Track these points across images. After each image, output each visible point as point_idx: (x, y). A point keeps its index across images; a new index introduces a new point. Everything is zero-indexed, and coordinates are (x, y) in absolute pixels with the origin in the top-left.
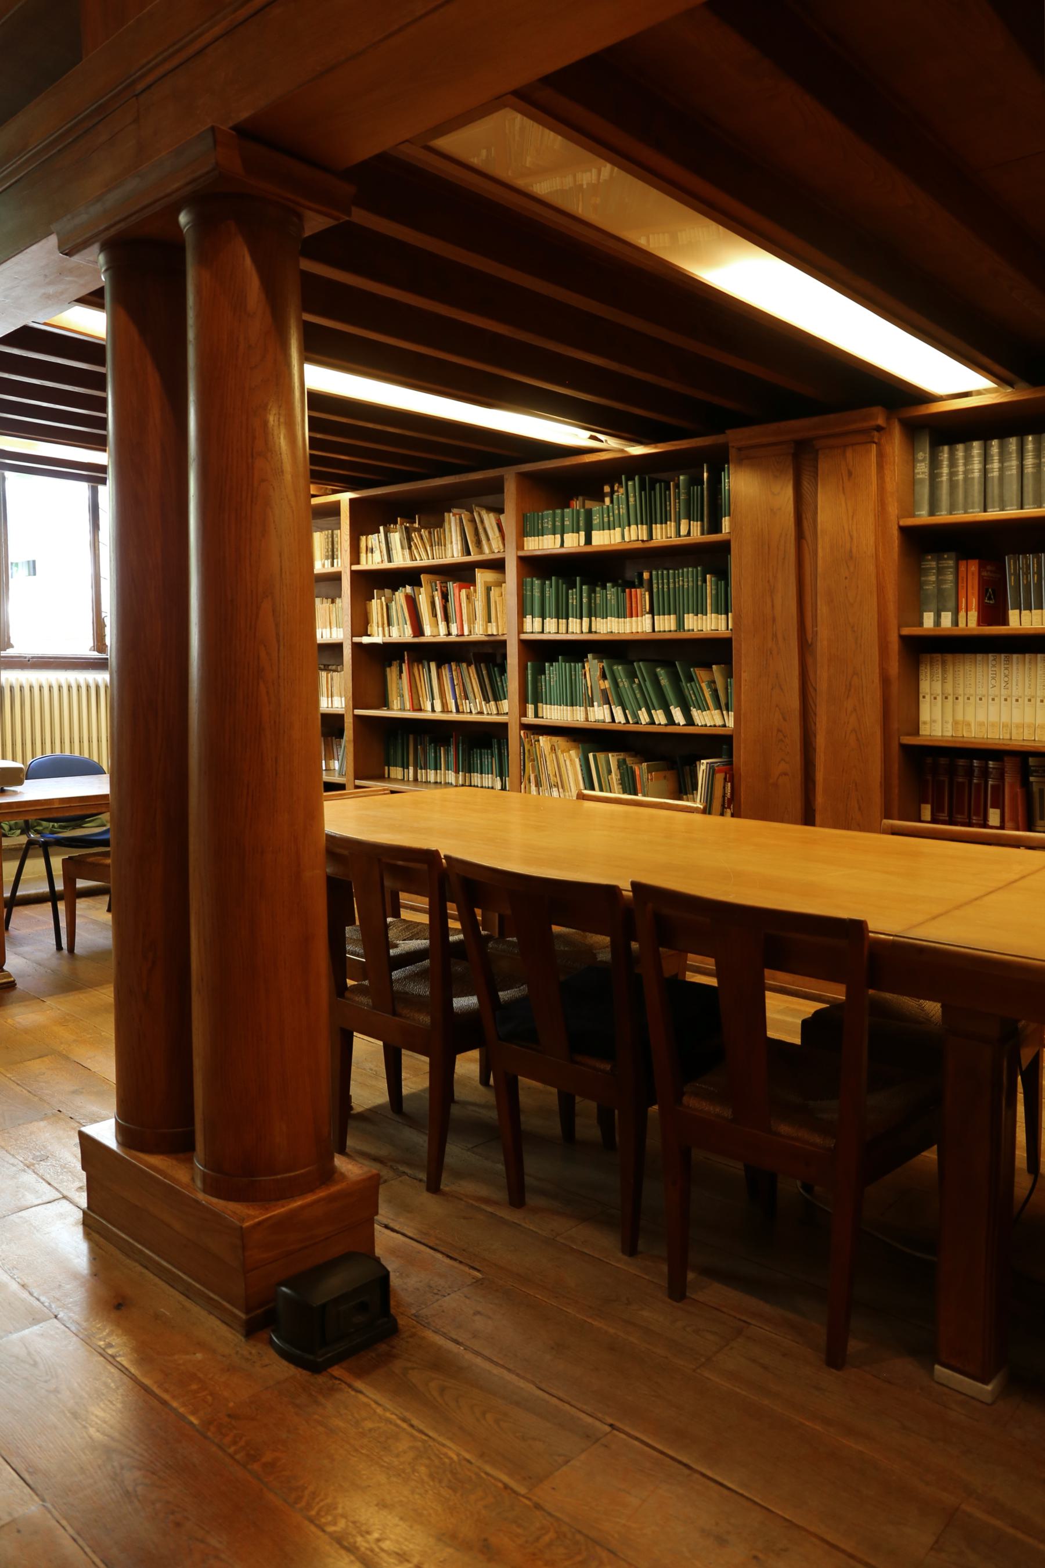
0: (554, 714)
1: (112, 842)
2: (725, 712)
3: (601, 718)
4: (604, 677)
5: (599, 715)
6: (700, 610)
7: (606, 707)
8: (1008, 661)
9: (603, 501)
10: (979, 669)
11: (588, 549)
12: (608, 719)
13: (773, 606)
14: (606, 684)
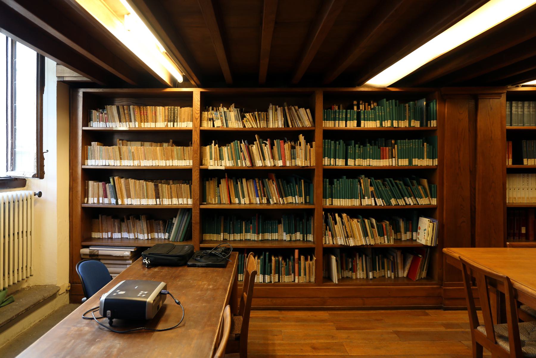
3: (370, 203)
4: (371, 185)
5: (368, 202)
6: (421, 157)
7: (373, 199)
8: (528, 176)
9: (353, 109)
10: (526, 179)
11: (358, 128)
12: (374, 204)
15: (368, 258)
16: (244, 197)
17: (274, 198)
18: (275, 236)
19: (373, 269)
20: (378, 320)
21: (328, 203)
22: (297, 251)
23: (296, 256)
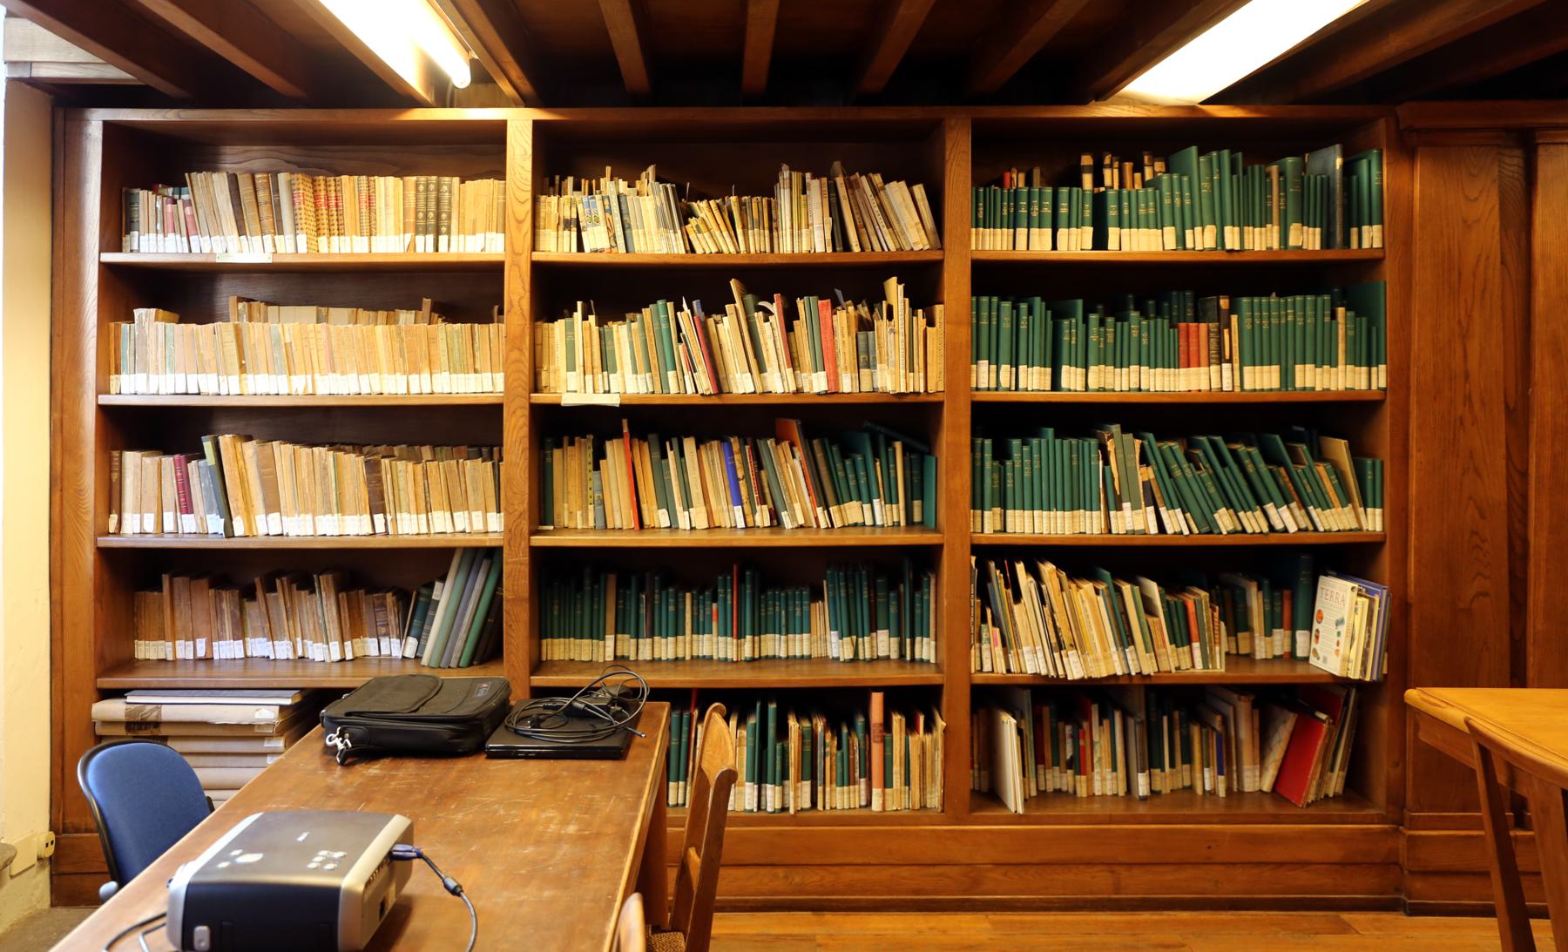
0: (1028, 524)
1: (1551, 912)
2: (1361, 510)
3: (1139, 526)
4: (1144, 460)
5: (1133, 521)
6: (1326, 358)
9: (1079, 184)
11: (1099, 255)
12: (1153, 529)
13: (1465, 356)
14: (1146, 474)
15: (1131, 722)
16: (688, 505)
17: (797, 506)
18: (800, 645)
22: (877, 699)
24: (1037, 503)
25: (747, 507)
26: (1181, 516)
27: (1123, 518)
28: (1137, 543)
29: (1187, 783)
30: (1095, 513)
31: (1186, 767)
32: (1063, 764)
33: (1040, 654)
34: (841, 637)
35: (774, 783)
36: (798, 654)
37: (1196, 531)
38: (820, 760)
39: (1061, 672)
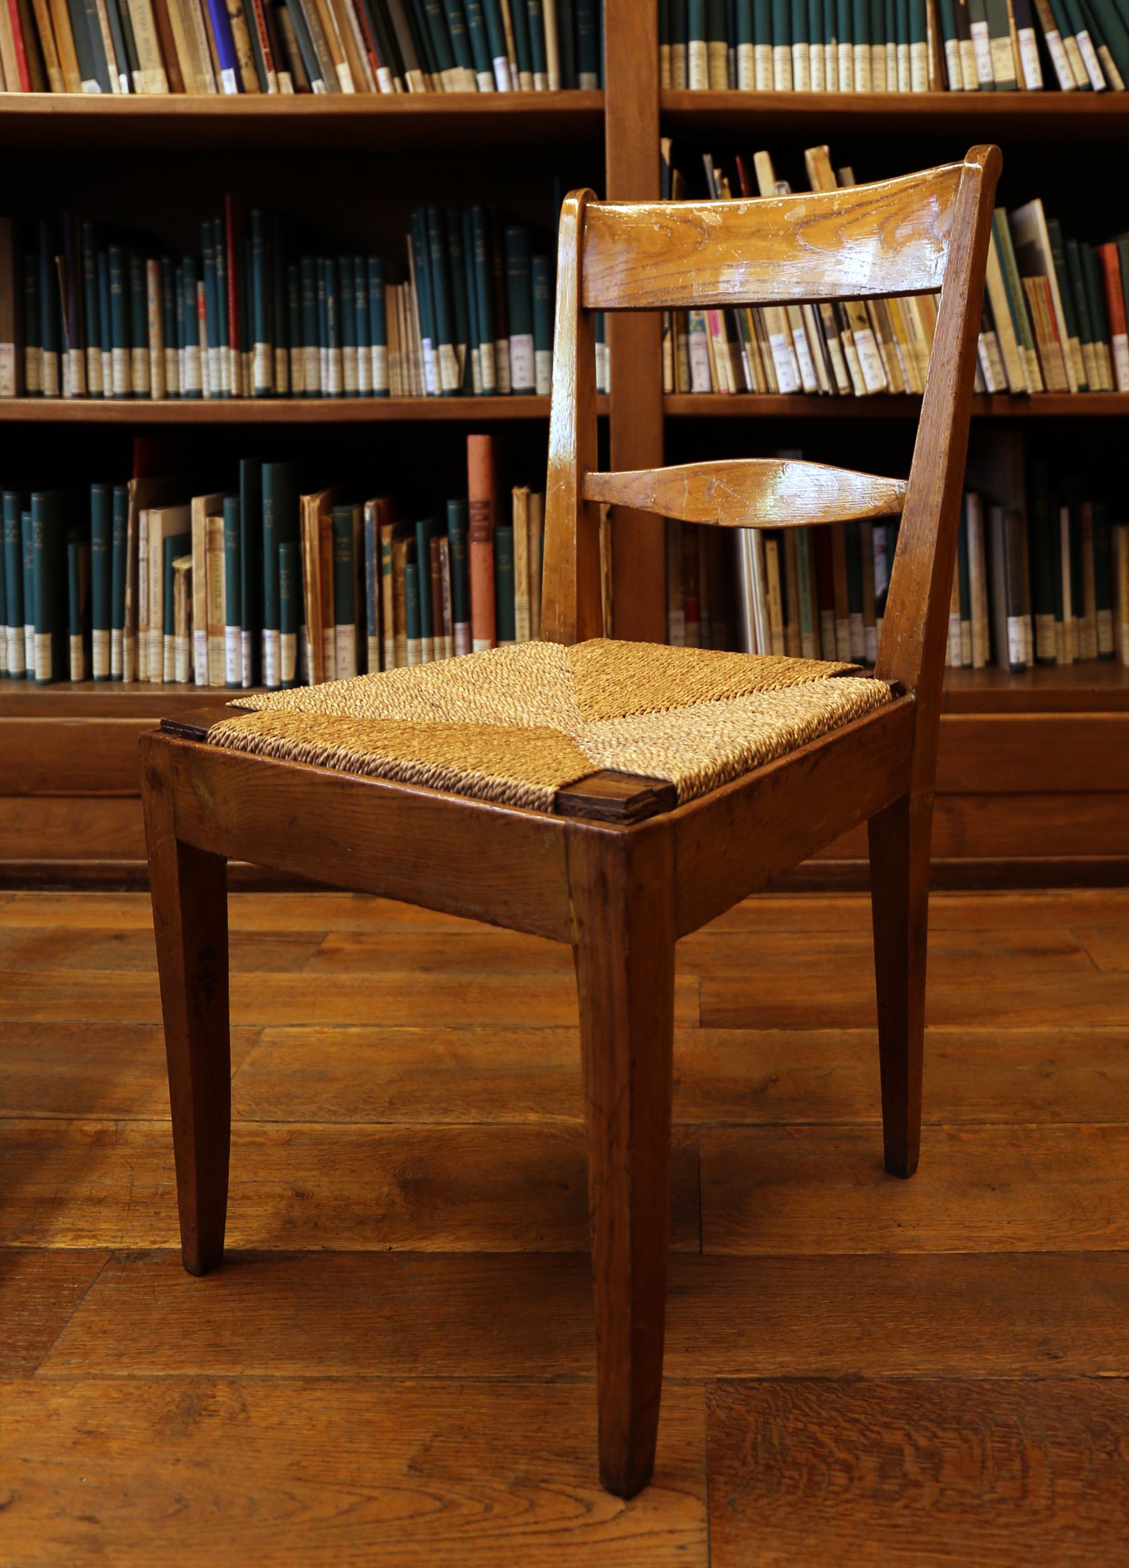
3: (1006, 74)
12: (1033, 80)
15: (997, 513)
16: (130, 64)
17: (343, 70)
18: (366, 370)
19: (1038, 602)
20: (300, 1480)
21: (698, 70)
22: (477, 447)
23: (478, 485)
24: (798, 29)
25: (247, 74)
26: (1087, 49)
27: (972, 55)
28: (998, 107)
29: (1106, 647)
30: (916, 48)
31: (1105, 614)
32: (869, 607)
33: (801, 347)
34: (435, 346)
35: (276, 626)
36: (362, 387)
37: (1119, 84)
38: (371, 582)
39: (842, 382)
